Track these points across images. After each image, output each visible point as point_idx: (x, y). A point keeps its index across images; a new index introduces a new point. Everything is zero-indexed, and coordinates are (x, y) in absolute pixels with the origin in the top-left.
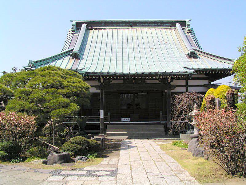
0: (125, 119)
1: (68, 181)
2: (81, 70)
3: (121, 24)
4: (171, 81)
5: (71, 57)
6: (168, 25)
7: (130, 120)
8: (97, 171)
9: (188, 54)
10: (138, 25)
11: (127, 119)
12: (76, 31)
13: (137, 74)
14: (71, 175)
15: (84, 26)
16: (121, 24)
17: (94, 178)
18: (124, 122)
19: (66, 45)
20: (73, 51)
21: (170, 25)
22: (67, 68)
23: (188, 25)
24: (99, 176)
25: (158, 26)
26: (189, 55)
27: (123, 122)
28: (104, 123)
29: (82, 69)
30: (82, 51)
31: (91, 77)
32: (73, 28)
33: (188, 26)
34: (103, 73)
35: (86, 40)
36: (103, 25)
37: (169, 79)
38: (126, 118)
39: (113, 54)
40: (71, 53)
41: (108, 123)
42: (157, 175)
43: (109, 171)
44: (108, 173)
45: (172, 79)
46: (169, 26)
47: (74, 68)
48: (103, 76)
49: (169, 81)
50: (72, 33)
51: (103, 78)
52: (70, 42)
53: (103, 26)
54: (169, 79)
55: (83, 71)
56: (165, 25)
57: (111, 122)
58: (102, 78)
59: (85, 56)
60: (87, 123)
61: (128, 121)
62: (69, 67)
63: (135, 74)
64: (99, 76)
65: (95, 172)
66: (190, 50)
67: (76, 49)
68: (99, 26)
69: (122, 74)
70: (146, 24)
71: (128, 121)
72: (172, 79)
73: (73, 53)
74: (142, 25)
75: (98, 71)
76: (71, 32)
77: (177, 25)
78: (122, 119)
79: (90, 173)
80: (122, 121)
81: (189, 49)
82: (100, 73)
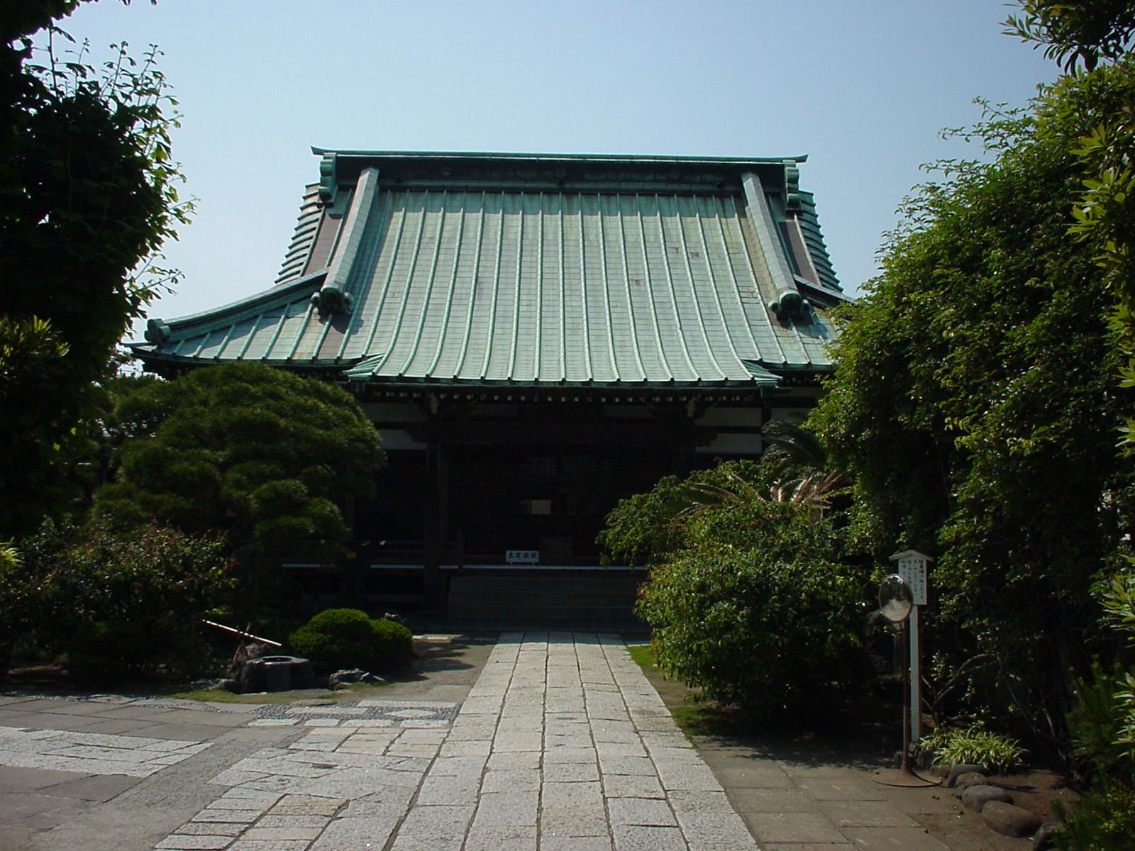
0: (518, 555)
1: (313, 728)
2: (354, 362)
3: (518, 174)
4: (699, 414)
5: (316, 310)
6: (709, 178)
7: (536, 560)
8: (399, 709)
9: (774, 307)
10: (587, 176)
11: (526, 556)
12: (334, 196)
13: (566, 386)
14: (321, 716)
15: (366, 180)
16: (518, 174)
17: (388, 722)
18: (514, 564)
19: (293, 264)
20: (325, 286)
21: (719, 179)
22: (301, 354)
23: (789, 181)
24: (402, 719)
25: (670, 181)
26: (780, 308)
27: (512, 567)
28: (441, 567)
29: (359, 360)
30: (358, 285)
31: (393, 394)
32: (322, 184)
33: (791, 186)
34: (437, 380)
35: (374, 239)
36: (447, 174)
37: (691, 409)
38: (523, 553)
39: (480, 299)
40: (316, 295)
41: (454, 570)
42: (571, 719)
43: (433, 710)
44: (431, 713)
45: (702, 406)
46: (712, 183)
47: (328, 355)
48: (438, 391)
49: (690, 414)
50: (319, 206)
51: (438, 398)
52: (311, 242)
53: (446, 178)
54: (691, 409)
55: (359, 371)
56: (698, 178)
57: (465, 567)
58: (434, 398)
59: (369, 313)
60: (373, 566)
61: (530, 564)
62: (307, 351)
63: (557, 385)
64: (424, 391)
65: (391, 711)
66: (783, 287)
67: (335, 275)
68: (432, 179)
69: (508, 384)
70: (622, 175)
71: (530, 564)
72: (702, 406)
73: (322, 294)
74: (603, 176)
75: (418, 372)
76: (316, 199)
77: (750, 185)
78: (508, 553)
79: (374, 713)
80: (508, 559)
81: (778, 286)
82: (428, 378)
